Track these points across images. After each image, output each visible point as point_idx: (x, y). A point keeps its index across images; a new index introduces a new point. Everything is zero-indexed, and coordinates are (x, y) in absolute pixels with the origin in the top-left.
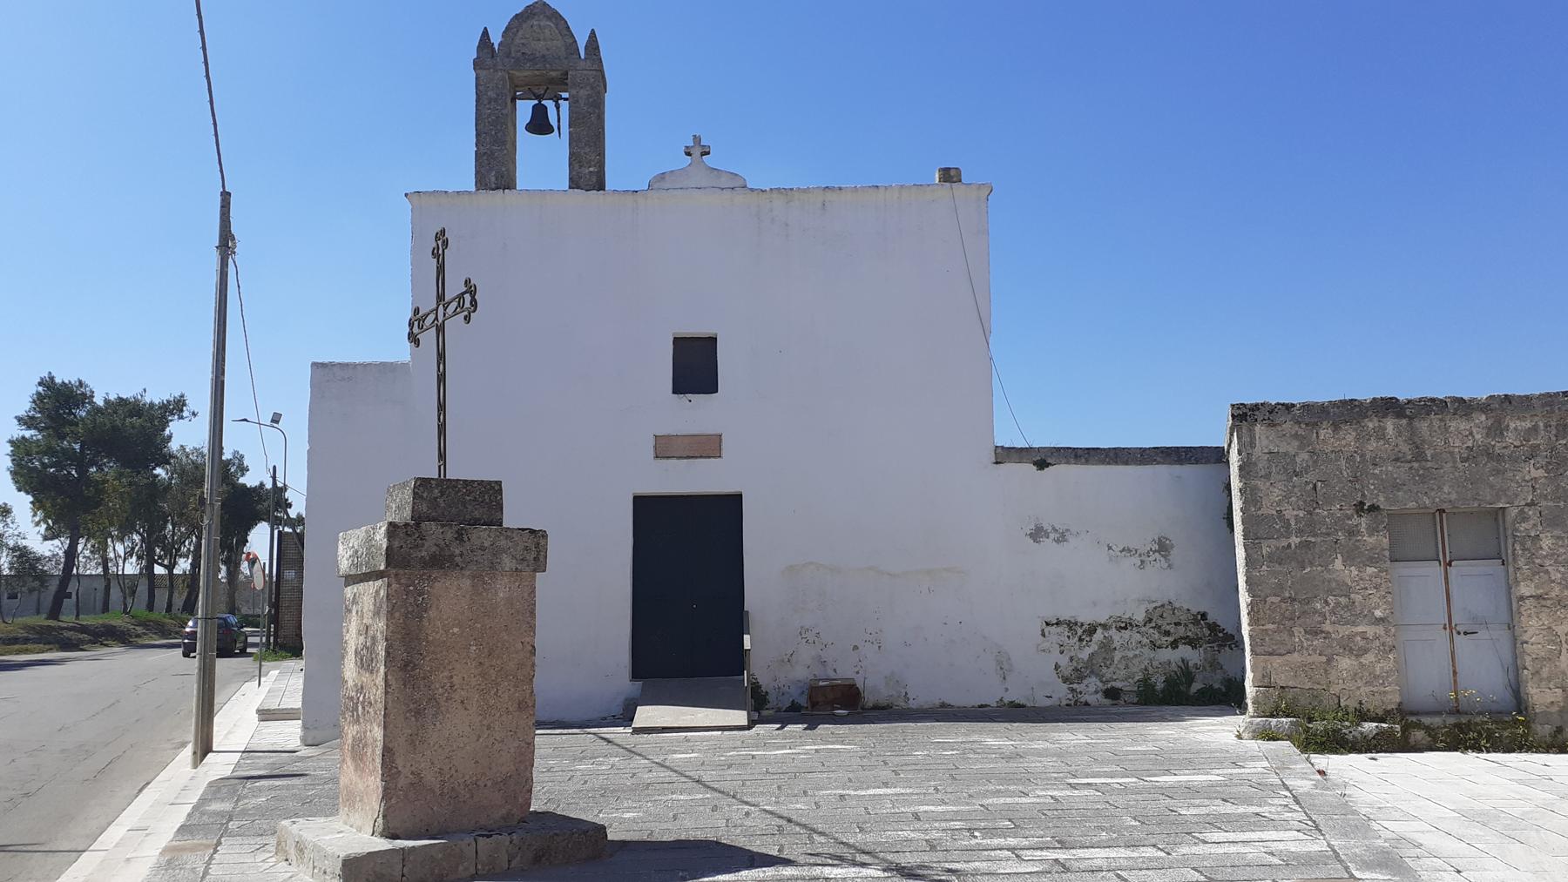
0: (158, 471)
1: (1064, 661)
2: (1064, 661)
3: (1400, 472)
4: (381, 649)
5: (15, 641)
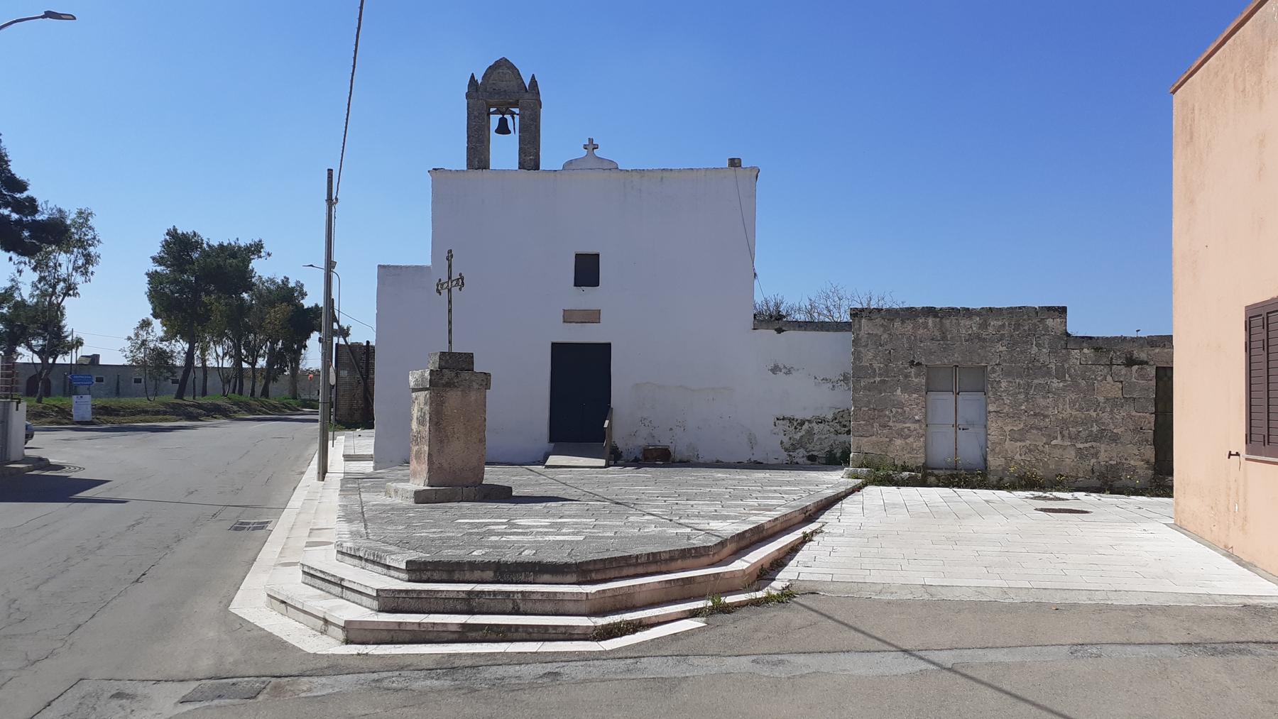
0: (245, 295)
1: (786, 439)
2: (786, 439)
3: (934, 346)
4: (427, 417)
5: (157, 413)
